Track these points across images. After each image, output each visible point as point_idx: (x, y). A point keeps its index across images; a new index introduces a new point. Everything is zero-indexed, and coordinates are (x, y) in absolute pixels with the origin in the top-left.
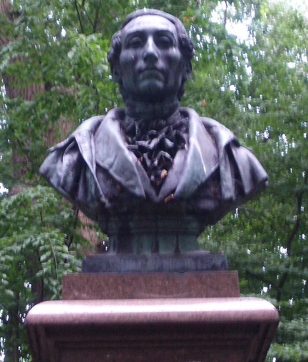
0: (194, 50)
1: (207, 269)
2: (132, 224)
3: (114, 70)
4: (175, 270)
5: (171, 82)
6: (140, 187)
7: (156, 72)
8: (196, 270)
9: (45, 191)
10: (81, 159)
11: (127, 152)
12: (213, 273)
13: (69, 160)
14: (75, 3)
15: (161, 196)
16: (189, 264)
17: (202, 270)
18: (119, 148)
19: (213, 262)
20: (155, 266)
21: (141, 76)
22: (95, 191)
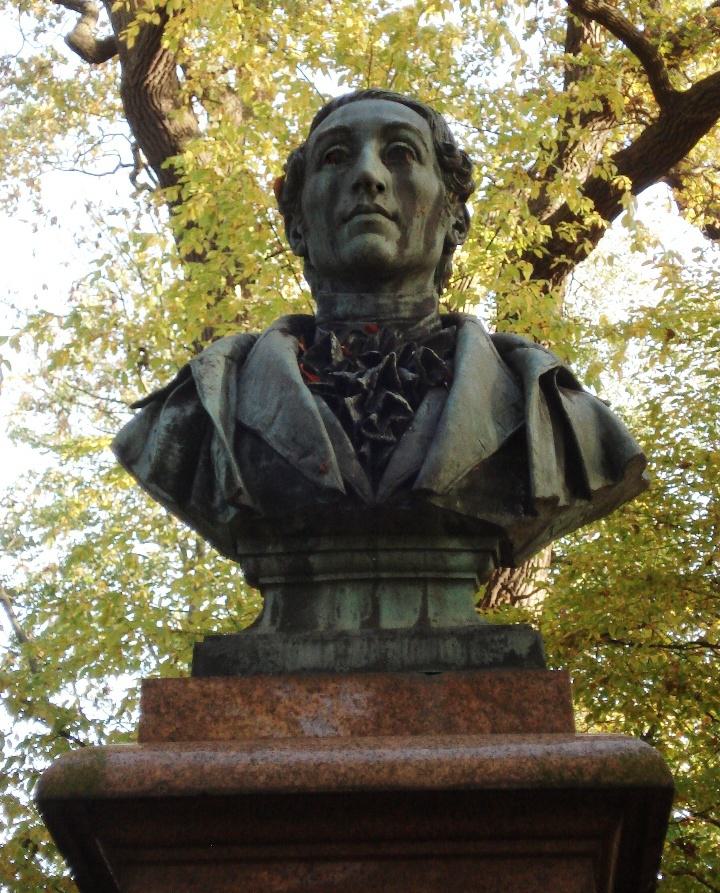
0: (306, 13)
1: (494, 664)
2: (315, 561)
3: (292, 230)
4: (414, 667)
5: (416, 245)
6: (336, 465)
7: (380, 218)
8: (469, 666)
9: (44, 348)
10: (202, 415)
11: (306, 392)
12: (507, 674)
13: (174, 419)
14: (716, 706)
15: (382, 490)
16: (450, 652)
17: (482, 666)
18: (287, 383)
19: (510, 647)
20: (367, 658)
21: (346, 230)
22: (226, 483)
